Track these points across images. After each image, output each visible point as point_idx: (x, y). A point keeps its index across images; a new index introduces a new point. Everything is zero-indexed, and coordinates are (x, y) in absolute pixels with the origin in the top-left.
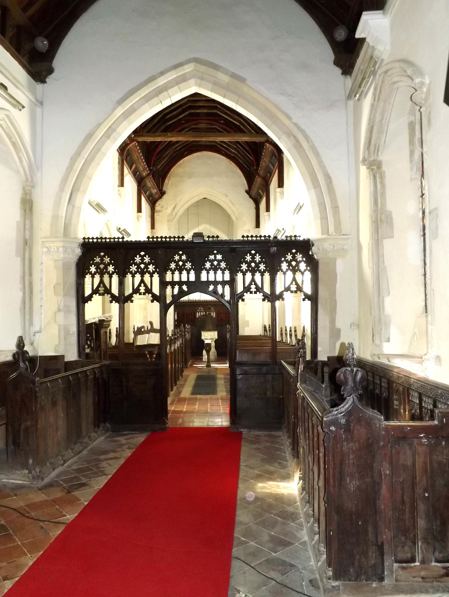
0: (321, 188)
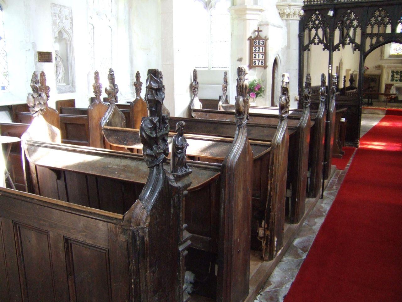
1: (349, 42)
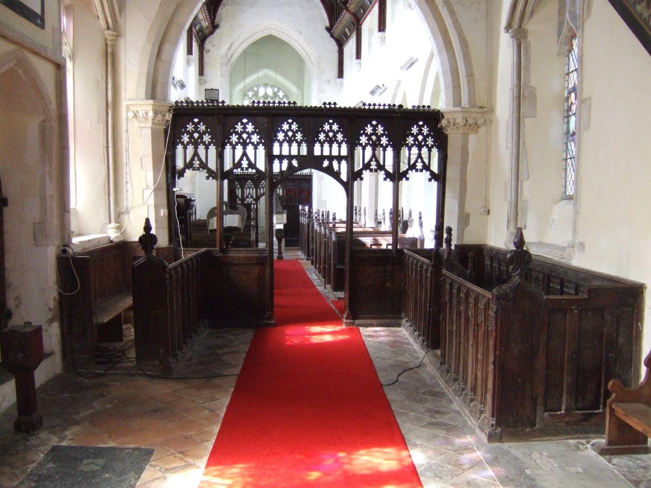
0: (454, 52)
1: (239, 169)
